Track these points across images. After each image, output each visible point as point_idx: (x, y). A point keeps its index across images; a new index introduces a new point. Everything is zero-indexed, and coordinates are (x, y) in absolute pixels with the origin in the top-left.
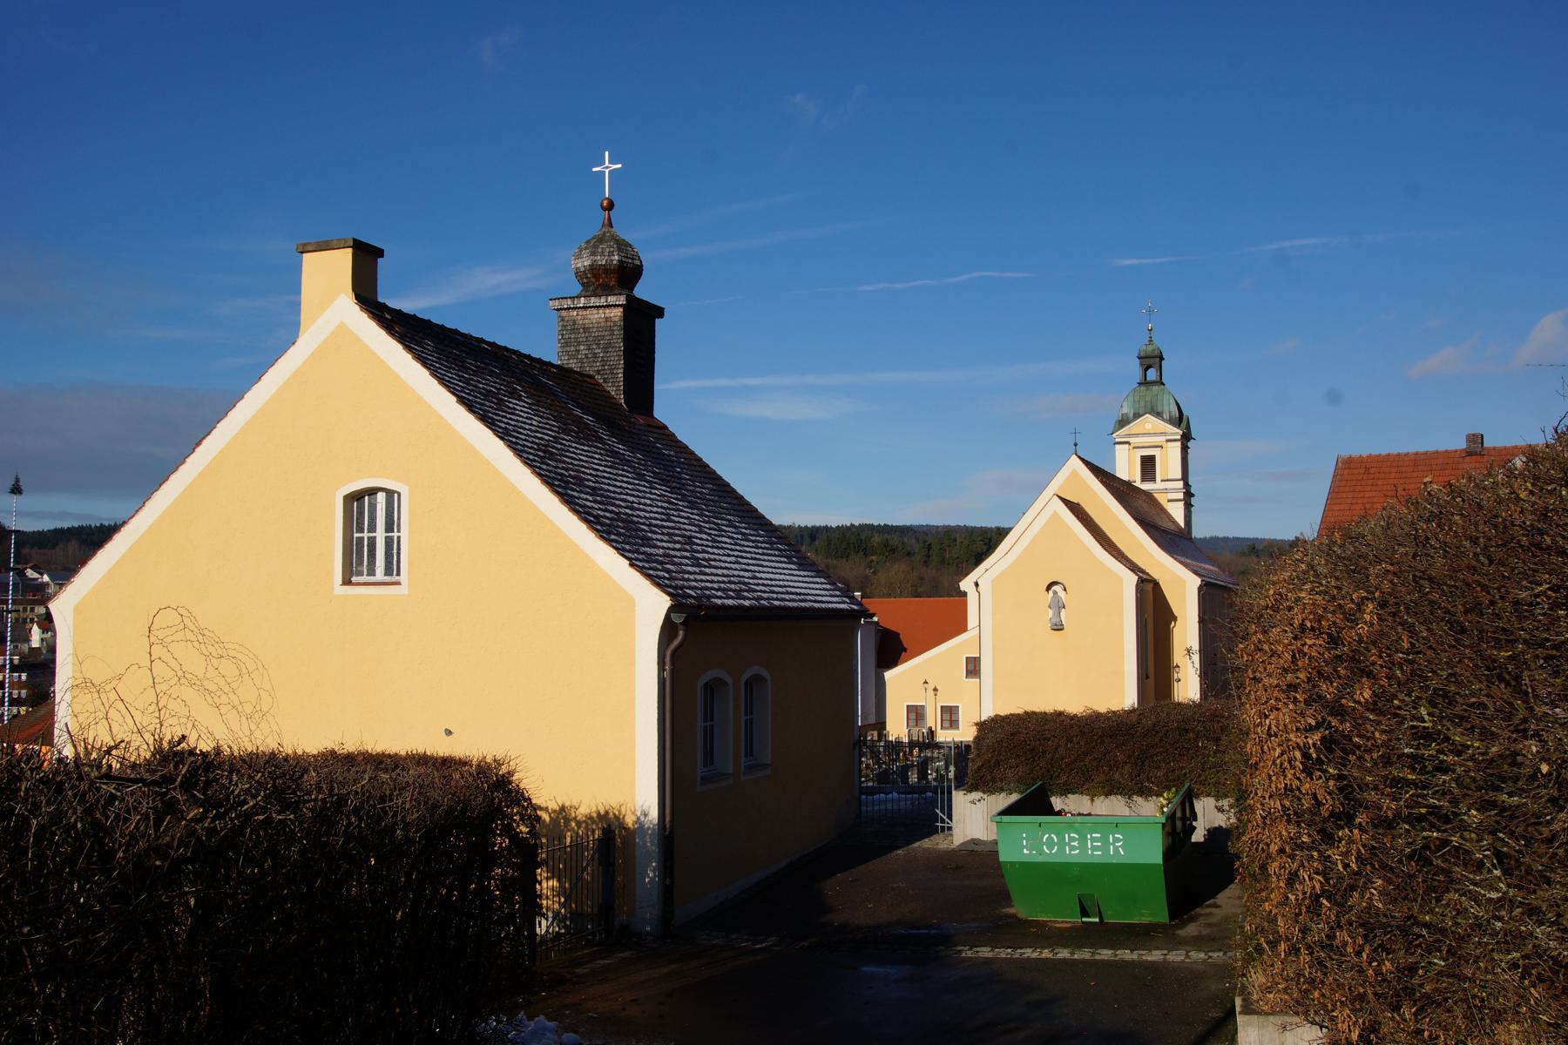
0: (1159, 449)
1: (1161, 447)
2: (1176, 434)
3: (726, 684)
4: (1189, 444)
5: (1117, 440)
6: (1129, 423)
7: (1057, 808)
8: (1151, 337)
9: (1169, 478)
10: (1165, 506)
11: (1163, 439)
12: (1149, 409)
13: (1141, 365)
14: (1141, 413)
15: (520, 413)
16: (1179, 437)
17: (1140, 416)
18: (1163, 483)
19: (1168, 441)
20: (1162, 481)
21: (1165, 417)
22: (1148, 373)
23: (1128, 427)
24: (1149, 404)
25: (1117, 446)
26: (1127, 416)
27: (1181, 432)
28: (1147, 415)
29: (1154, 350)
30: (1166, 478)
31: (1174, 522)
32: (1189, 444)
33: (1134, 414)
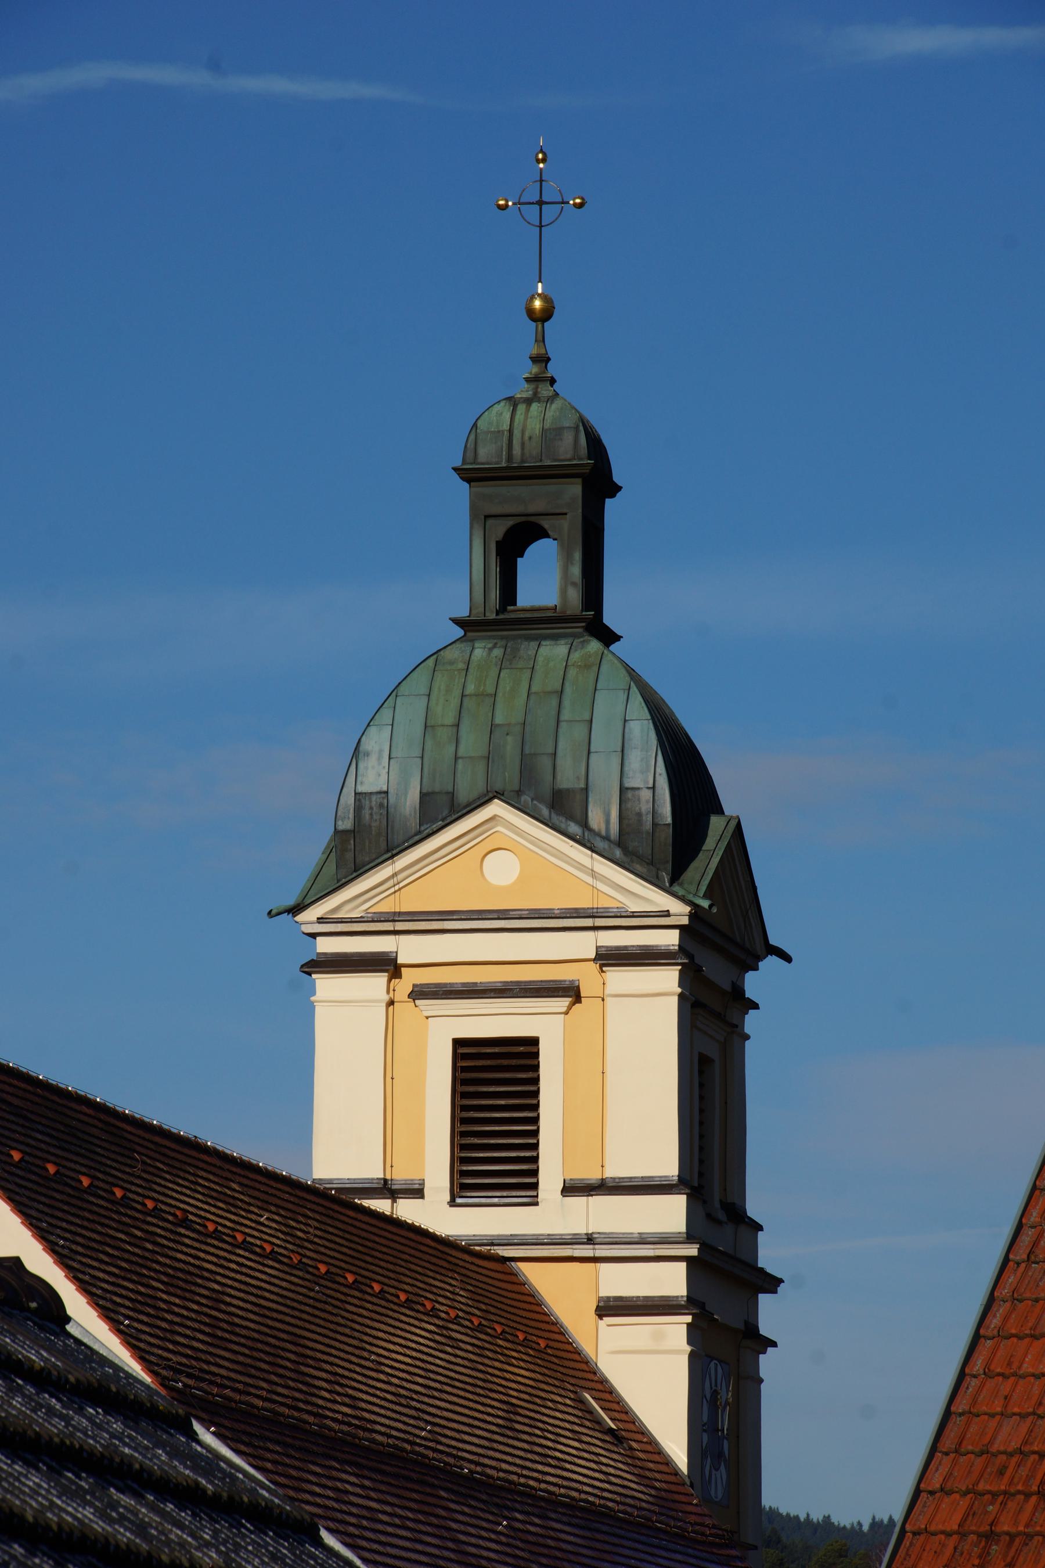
0: (561, 1004)
1: (572, 992)
2: (656, 919)
3: (713, 1061)
4: (753, 984)
5: (326, 946)
6: (392, 850)
7: (502, 404)
8: (542, 360)
9: (614, 1170)
10: (587, 1347)
11: (585, 945)
12: (509, 775)
13: (481, 517)
14: (464, 794)
15: (110, 1206)
16: (671, 939)
17: (458, 811)
18: (578, 1202)
19: (608, 958)
20: (570, 1189)
21: (596, 819)
22: (523, 565)
23: (385, 872)
24: (510, 746)
25: (326, 985)
26: (386, 809)
27: (680, 911)
28: (496, 808)
29: (550, 435)
30: (593, 1175)
31: (667, 1461)
32: (753, 984)
33: (425, 797)
